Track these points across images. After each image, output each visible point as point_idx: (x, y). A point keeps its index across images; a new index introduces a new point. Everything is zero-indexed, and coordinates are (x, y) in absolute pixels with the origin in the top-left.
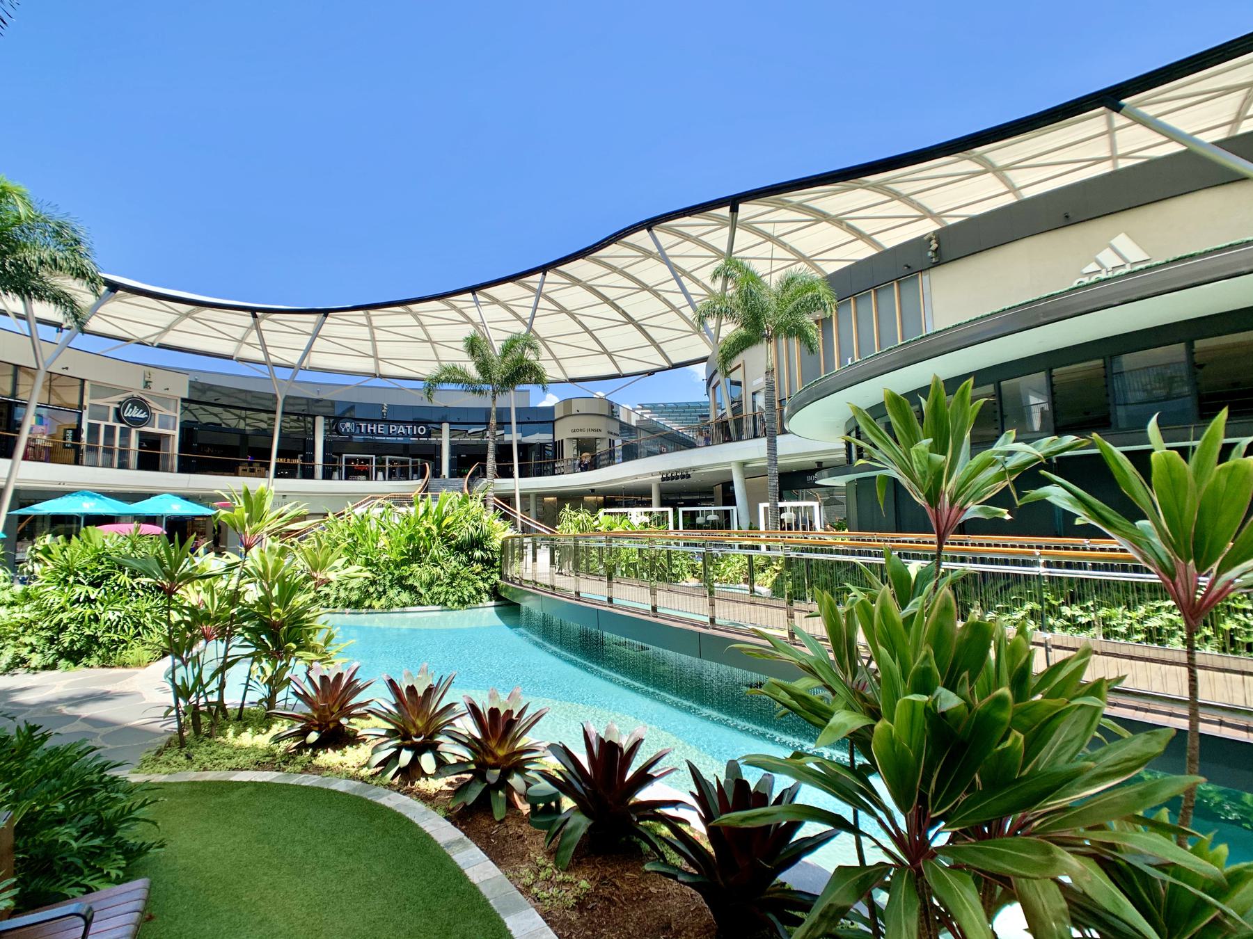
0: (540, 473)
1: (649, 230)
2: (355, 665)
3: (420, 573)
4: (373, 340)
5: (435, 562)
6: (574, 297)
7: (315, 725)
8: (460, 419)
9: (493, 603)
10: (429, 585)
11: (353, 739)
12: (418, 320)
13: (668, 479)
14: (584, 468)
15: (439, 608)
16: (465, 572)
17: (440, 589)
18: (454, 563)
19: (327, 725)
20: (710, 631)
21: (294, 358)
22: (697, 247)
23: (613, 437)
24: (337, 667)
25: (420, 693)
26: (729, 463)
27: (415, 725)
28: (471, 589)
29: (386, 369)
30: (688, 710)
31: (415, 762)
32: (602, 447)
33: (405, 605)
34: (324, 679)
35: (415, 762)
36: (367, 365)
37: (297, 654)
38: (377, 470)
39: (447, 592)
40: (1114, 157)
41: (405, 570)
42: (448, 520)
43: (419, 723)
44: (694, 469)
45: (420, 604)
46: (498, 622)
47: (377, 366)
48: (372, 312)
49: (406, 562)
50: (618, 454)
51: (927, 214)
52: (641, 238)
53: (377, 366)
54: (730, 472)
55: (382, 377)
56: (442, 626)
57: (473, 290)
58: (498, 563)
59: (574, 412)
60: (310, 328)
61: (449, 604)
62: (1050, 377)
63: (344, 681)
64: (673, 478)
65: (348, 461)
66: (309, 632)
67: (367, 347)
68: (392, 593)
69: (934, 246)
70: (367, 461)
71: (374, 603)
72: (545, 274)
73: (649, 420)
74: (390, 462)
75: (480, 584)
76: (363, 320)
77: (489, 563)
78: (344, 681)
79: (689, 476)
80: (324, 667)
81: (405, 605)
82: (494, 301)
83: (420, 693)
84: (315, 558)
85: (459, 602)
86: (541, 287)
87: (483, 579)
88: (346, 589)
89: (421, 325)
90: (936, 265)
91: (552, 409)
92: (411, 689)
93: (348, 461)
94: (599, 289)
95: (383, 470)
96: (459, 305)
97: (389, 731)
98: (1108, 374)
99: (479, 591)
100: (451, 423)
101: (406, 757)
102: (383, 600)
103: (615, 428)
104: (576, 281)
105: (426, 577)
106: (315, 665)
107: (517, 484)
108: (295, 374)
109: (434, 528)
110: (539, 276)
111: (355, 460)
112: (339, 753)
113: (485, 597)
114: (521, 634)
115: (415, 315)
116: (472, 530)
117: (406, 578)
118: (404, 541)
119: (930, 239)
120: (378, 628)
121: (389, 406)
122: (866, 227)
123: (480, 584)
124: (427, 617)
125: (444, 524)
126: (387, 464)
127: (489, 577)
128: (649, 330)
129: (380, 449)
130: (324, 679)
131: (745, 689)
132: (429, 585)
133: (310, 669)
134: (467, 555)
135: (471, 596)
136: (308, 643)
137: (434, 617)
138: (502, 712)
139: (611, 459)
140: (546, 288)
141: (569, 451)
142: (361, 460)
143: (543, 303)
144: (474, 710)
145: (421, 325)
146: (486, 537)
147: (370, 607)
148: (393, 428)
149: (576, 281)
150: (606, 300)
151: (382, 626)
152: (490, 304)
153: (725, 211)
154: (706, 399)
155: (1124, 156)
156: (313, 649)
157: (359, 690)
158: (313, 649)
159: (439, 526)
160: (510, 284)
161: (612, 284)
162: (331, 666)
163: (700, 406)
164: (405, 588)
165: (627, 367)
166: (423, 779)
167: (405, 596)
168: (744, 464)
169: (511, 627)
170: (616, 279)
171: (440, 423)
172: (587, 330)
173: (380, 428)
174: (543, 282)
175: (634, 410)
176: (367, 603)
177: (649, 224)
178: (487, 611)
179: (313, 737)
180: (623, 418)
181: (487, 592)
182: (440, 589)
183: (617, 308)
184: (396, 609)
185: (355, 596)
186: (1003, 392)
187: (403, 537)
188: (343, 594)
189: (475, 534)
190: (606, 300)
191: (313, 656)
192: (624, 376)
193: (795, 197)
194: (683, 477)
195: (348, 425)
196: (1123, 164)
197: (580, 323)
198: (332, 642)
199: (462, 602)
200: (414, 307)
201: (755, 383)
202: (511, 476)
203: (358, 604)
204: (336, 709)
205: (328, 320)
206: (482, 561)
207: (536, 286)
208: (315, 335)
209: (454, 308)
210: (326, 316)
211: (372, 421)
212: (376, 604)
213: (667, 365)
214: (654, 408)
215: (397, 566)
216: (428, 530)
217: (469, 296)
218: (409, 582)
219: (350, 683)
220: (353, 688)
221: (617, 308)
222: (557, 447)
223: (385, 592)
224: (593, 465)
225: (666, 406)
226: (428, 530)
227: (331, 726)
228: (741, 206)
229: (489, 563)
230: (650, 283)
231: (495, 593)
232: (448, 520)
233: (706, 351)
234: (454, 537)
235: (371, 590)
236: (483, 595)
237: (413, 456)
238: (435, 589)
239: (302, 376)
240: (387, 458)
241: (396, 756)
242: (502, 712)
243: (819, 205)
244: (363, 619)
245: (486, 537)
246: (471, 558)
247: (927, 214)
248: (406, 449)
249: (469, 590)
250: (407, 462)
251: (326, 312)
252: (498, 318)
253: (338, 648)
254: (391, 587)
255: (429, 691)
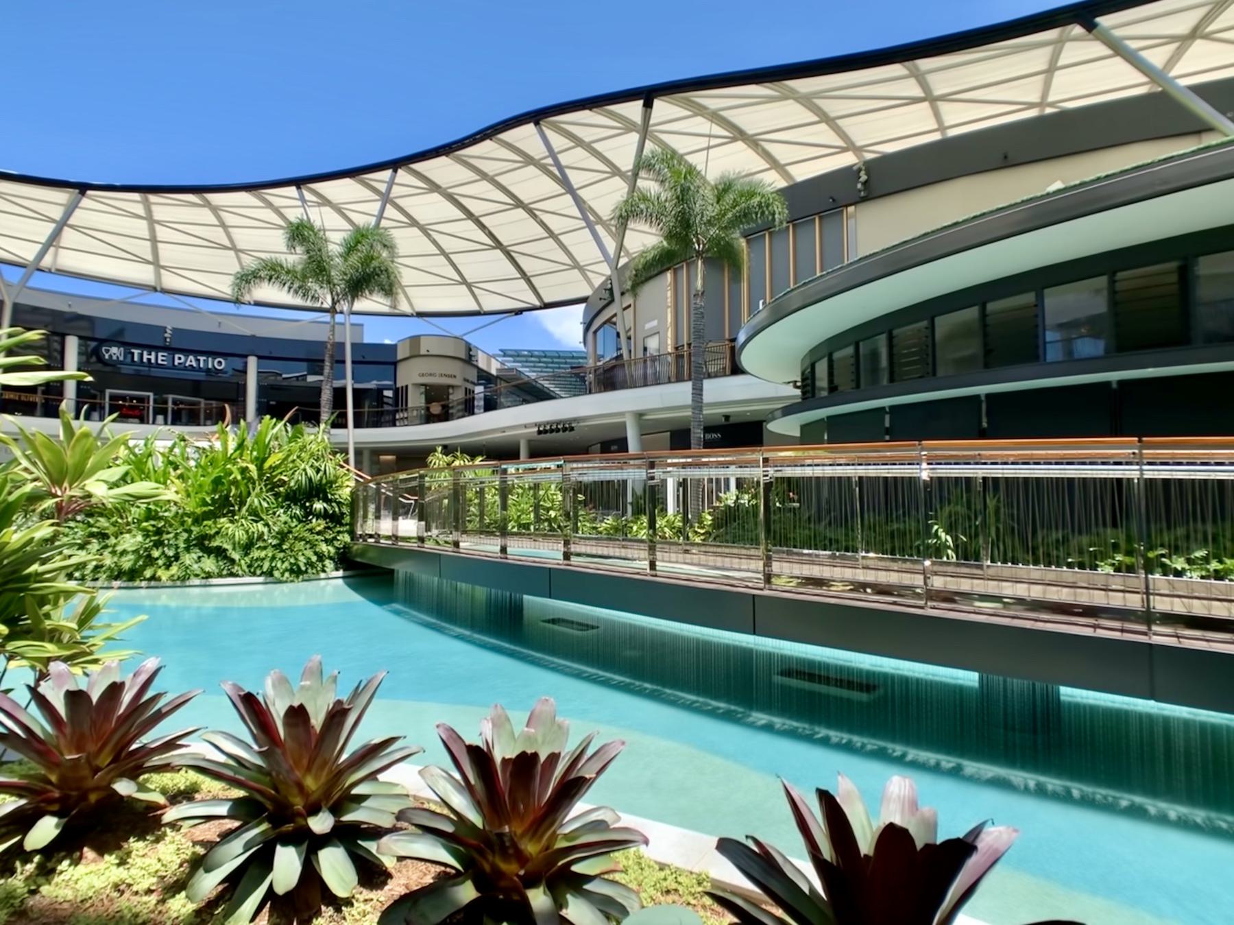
0: (377, 424)
1: (537, 124)
2: (151, 664)
3: (232, 530)
4: (154, 240)
5: (256, 515)
6: (430, 208)
7: (51, 801)
8: (272, 351)
9: (340, 573)
10: (247, 547)
11: (145, 821)
12: (219, 218)
13: (545, 432)
14: (429, 418)
15: (261, 579)
16: (299, 529)
17: (263, 554)
18: (284, 518)
19: (84, 797)
20: (766, 592)
21: (28, 253)
22: (612, 138)
23: (470, 386)
24: (107, 670)
25: (317, 720)
26: (622, 414)
27: (301, 787)
28: (309, 553)
29: (170, 281)
30: (728, 717)
31: (310, 874)
32: (457, 396)
33: (209, 575)
34: (76, 698)
35: (310, 874)
36: (144, 274)
37: (10, 646)
38: (156, 413)
39: (273, 558)
40: (1042, 104)
41: (209, 527)
42: (272, 461)
43: (310, 783)
44: (576, 420)
45: (232, 575)
46: (355, 597)
47: (158, 276)
48: (153, 198)
49: (212, 516)
50: (479, 403)
51: (850, 146)
52: (525, 135)
53: (158, 276)
54: (623, 426)
55: (165, 291)
56: (265, 603)
57: (298, 182)
58: (347, 519)
59: (423, 352)
60: (57, 213)
61: (277, 574)
62: (1112, 282)
63: (127, 698)
64: (552, 431)
65: (112, 398)
66: (43, 601)
67: (145, 249)
68: (188, 559)
69: (864, 177)
70: (141, 400)
71: (159, 573)
72: (395, 171)
73: (511, 369)
74: (175, 403)
75: (324, 547)
76: (139, 209)
77: (334, 519)
78: (127, 698)
79: (572, 429)
80: (77, 671)
81: (209, 575)
82: (325, 201)
83: (317, 720)
84: (58, 456)
85: (292, 571)
86: (389, 189)
87: (326, 541)
88: (114, 553)
89: (223, 225)
90: (864, 200)
91: (393, 348)
92: (297, 714)
93: (112, 398)
94: (462, 200)
95: (163, 412)
96: (277, 202)
97: (237, 802)
98: (1185, 276)
99: (321, 557)
100: (259, 357)
101: (287, 867)
102: (174, 569)
103: (473, 375)
104: (434, 187)
105: (240, 535)
106: (55, 667)
107: (353, 436)
108: (27, 277)
109: (252, 467)
110: (386, 174)
111: (123, 398)
112: (111, 859)
113: (329, 564)
114: (398, 613)
115: (215, 210)
116: (310, 472)
117: (211, 537)
118: (208, 488)
119: (860, 170)
120: (166, 608)
121: (174, 330)
122: (782, 153)
123: (324, 547)
124: (244, 592)
125: (266, 465)
126: (170, 405)
127: (335, 539)
128: (521, 260)
129: (161, 384)
130: (76, 698)
131: (778, 679)
132: (247, 547)
133: (43, 676)
134: (303, 507)
135: (309, 564)
136: (38, 620)
137: (254, 593)
138: (543, 758)
139: (469, 409)
140: (396, 190)
141: (416, 400)
142: (132, 398)
143: (390, 211)
144: (251, 706)
145: (223, 225)
146: (331, 483)
147: (153, 578)
148: (179, 359)
149: (434, 187)
150: (470, 215)
151: (173, 604)
152: (319, 205)
153: (633, 109)
154: (581, 347)
155: (1052, 105)
156: (53, 635)
157: (160, 716)
158: (53, 635)
159: (260, 469)
160: (347, 181)
161: (481, 197)
162: (91, 668)
163: (572, 355)
164: (209, 551)
165: (490, 303)
166: (327, 911)
167: (209, 564)
168: (640, 415)
169: (380, 602)
170: (484, 188)
171: (246, 356)
172: (443, 253)
173: (162, 358)
174: (391, 183)
175: (494, 356)
176: (148, 573)
177: (536, 117)
178: (332, 585)
179: (45, 830)
180: (482, 364)
181: (331, 558)
182: (263, 554)
183: (483, 227)
184: (197, 581)
185: (127, 563)
186: (989, 320)
187: (207, 480)
188: (108, 561)
189: (316, 478)
190: (470, 215)
191: (51, 649)
192: (486, 314)
193: (712, 99)
194: (565, 429)
195: (114, 350)
196: (1049, 111)
197: (435, 243)
198: (95, 622)
199: (296, 572)
200: (215, 198)
201: (648, 326)
202: (345, 426)
203: (132, 575)
204: (104, 760)
205: (85, 202)
206: (325, 515)
207: (383, 188)
208: (62, 224)
209: (270, 205)
210: (83, 193)
211: (151, 348)
212: (163, 574)
213: (537, 303)
214: (517, 355)
215: (198, 520)
216: (244, 471)
217: (292, 191)
218: (215, 544)
219: (137, 706)
220: (145, 712)
221: (483, 227)
222: (400, 395)
223: (177, 557)
224: (445, 417)
225: (531, 354)
226: (244, 471)
227: (93, 798)
228: (657, 103)
229: (334, 519)
230: (525, 199)
231: (345, 560)
232: (272, 461)
233: (586, 291)
234: (283, 483)
235: (156, 553)
236: (327, 562)
237: (206, 399)
238: (256, 554)
239: (38, 281)
240: (170, 397)
241: (261, 861)
242: (543, 758)
243: (737, 117)
244: (142, 594)
245: (331, 483)
246: (309, 512)
247: (850, 146)
248: (196, 388)
249: (304, 555)
250: (199, 403)
251: (83, 188)
252: (341, 210)
253: (109, 633)
254: (188, 549)
255: (337, 715)
